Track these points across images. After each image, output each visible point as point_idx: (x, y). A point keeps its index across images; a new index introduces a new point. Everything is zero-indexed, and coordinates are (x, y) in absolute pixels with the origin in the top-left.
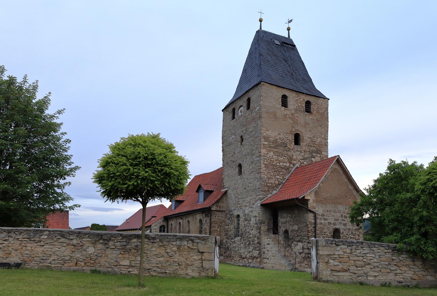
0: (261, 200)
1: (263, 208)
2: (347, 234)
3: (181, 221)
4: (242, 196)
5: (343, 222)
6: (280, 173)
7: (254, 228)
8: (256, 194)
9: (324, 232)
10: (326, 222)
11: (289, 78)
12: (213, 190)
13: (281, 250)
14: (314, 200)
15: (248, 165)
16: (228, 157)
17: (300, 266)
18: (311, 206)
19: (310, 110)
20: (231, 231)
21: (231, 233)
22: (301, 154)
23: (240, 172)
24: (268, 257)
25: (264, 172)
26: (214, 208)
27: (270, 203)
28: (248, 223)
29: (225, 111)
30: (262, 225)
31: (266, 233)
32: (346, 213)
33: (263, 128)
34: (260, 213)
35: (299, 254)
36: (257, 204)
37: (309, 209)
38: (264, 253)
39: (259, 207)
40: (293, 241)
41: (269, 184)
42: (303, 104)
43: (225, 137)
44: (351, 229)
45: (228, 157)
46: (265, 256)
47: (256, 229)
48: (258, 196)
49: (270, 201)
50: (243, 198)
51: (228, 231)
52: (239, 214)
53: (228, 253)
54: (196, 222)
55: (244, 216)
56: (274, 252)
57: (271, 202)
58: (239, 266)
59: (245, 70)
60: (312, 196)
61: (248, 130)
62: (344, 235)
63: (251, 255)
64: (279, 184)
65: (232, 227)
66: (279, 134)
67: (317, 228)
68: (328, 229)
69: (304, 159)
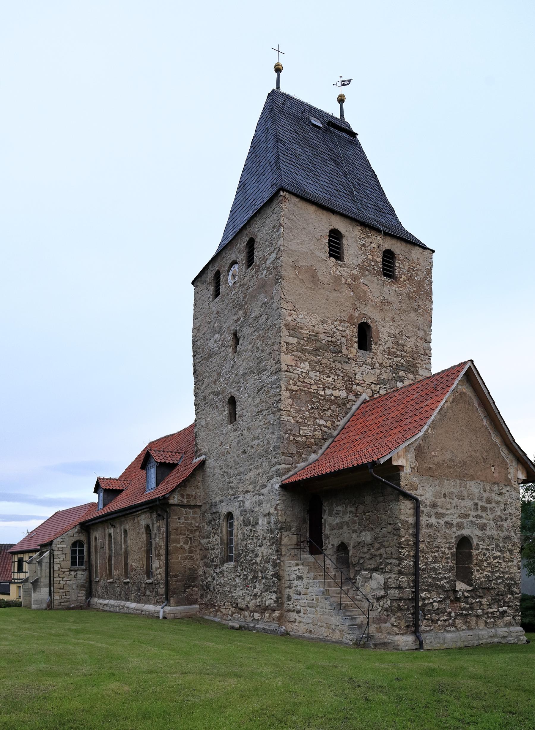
0: (280, 474)
1: (286, 493)
2: (487, 550)
3: (111, 531)
4: (236, 469)
5: (479, 521)
6: (326, 412)
7: (264, 542)
8: (270, 461)
9: (438, 547)
10: (442, 522)
11: (344, 199)
12: (176, 462)
13: (331, 592)
14: (414, 468)
15: (249, 396)
16: (206, 384)
17: (379, 630)
18: (407, 482)
19: (393, 272)
20: (214, 549)
21: (215, 553)
22: (373, 371)
23: (233, 417)
24: (298, 607)
25: (289, 408)
26: (176, 499)
27: (303, 480)
28: (251, 530)
29: (199, 284)
30: (285, 534)
31: (292, 552)
32: (484, 500)
33: (284, 304)
34: (279, 507)
35: (375, 601)
36: (272, 486)
37: (402, 489)
38: (289, 598)
39: (277, 492)
40: (360, 570)
41: (299, 439)
42: (378, 257)
43: (199, 342)
44: (495, 537)
45: (206, 384)
46: (292, 606)
47: (269, 544)
48: (273, 465)
49: (301, 477)
50: (239, 474)
51: (208, 549)
52: (230, 510)
53: (209, 597)
54: (139, 533)
55: (241, 515)
56: (314, 597)
57: (307, 479)
58: (232, 628)
59: (242, 187)
60: (409, 458)
61: (249, 316)
62: (481, 552)
63: (259, 602)
64: (324, 439)
65: (216, 540)
66: (323, 322)
67: (420, 536)
68: (445, 538)
69: (380, 383)
